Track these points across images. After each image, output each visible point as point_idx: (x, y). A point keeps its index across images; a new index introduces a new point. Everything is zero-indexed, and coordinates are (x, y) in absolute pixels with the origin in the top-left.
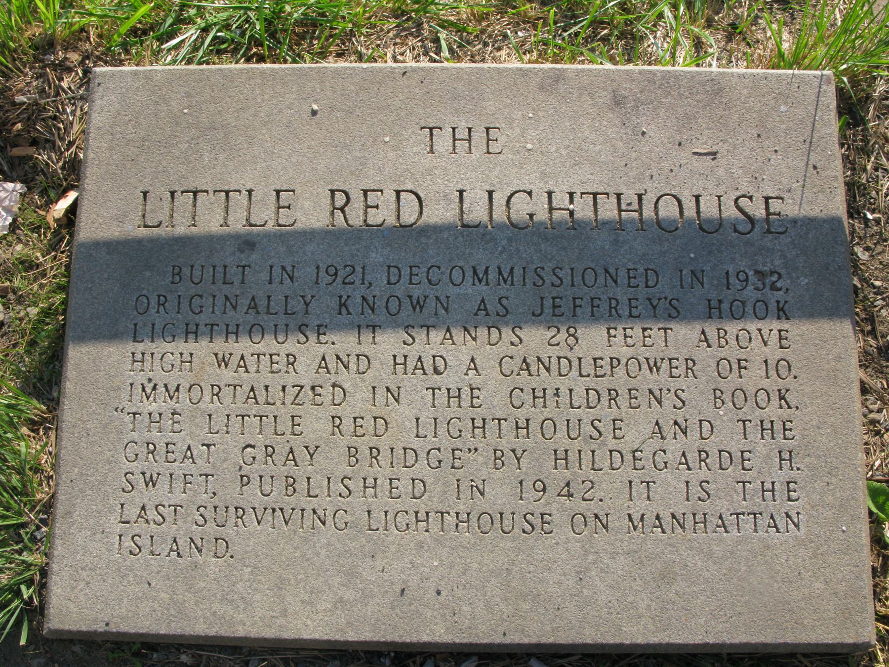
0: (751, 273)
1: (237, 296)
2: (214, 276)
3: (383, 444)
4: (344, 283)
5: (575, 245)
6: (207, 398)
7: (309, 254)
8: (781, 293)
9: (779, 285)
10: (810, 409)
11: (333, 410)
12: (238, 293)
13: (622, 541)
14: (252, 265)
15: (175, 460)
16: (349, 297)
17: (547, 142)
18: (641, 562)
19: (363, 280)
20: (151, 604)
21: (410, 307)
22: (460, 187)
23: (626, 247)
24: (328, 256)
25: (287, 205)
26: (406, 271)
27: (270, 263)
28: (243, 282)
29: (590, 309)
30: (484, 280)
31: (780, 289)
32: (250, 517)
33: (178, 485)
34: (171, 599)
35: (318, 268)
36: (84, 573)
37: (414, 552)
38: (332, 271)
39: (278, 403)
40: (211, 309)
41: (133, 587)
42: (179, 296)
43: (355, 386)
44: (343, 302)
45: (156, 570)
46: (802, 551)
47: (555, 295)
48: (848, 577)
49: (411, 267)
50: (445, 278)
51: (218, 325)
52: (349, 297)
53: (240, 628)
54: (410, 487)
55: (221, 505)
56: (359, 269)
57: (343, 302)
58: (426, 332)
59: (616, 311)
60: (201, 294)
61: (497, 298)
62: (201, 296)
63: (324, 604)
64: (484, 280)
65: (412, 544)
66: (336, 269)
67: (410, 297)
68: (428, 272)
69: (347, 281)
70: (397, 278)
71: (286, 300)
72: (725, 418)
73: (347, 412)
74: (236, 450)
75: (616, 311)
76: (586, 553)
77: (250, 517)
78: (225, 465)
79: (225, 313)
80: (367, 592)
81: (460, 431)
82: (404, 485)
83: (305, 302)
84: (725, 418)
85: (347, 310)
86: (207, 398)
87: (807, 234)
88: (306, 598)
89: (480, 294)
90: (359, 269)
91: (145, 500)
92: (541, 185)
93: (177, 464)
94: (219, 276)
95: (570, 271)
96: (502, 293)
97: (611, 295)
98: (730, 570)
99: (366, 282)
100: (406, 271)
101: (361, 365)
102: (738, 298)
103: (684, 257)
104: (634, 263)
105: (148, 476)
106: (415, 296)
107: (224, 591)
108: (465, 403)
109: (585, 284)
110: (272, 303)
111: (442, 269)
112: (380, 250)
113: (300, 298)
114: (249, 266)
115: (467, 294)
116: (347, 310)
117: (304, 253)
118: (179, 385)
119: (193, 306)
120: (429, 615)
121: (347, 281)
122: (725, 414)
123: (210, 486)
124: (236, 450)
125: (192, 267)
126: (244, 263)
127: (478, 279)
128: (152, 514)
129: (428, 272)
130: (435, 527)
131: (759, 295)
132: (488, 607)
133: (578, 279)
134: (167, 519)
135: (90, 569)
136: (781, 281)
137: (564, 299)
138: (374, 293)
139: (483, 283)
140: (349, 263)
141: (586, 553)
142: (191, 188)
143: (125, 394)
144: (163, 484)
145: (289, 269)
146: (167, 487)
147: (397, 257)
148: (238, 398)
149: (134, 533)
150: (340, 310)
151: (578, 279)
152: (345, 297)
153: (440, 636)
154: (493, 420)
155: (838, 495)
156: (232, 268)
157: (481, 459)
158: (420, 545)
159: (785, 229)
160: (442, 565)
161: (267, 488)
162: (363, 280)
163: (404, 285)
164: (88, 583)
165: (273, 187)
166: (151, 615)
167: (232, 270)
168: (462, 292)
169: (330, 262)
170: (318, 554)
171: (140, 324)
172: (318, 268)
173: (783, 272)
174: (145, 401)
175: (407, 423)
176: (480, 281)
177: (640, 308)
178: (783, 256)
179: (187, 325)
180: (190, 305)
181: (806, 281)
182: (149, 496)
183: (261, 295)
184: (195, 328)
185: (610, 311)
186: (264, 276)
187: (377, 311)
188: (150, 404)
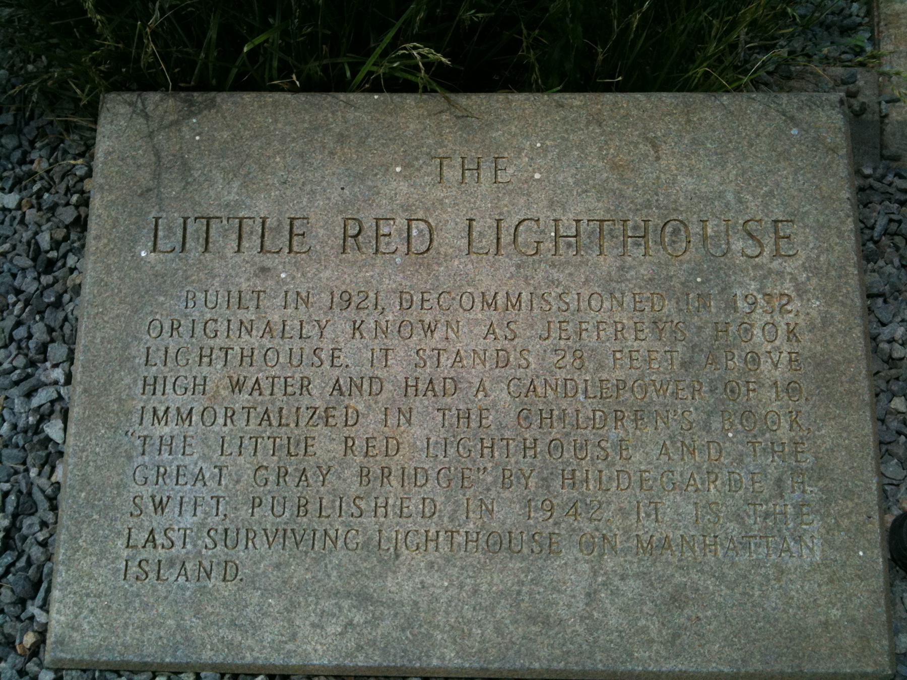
0: (759, 296)
1: (252, 321)
2: (229, 301)
3: (394, 464)
4: (357, 308)
5: (582, 271)
6: (221, 421)
7: (325, 280)
8: (791, 315)
9: (789, 308)
10: (823, 431)
11: (347, 432)
12: (253, 318)
13: (631, 562)
14: (268, 291)
15: (186, 483)
16: (362, 321)
17: (555, 170)
18: (652, 585)
19: (376, 305)
20: (155, 631)
21: (422, 332)
22: (469, 216)
23: (633, 273)
24: (344, 283)
25: (301, 232)
26: (417, 298)
27: (285, 288)
28: (258, 307)
29: (596, 333)
30: (493, 305)
31: (790, 312)
32: (260, 541)
33: (188, 508)
34: (178, 626)
35: (332, 293)
36: (89, 600)
37: (424, 572)
38: (346, 297)
39: (292, 425)
40: (226, 334)
41: (139, 613)
42: (194, 321)
43: (369, 407)
44: (357, 326)
45: (164, 595)
46: (818, 577)
47: (562, 320)
48: (865, 603)
49: (422, 293)
50: (456, 304)
51: (232, 349)
52: (362, 321)
53: (248, 655)
54: (421, 506)
55: (232, 527)
56: (372, 295)
57: (357, 326)
58: (61, 425)
59: (622, 334)
60: (215, 318)
61: (506, 323)
62: (216, 321)
63: (333, 628)
64: (493, 305)
65: (422, 564)
66: (350, 294)
67: (422, 321)
68: (439, 298)
69: (361, 306)
70: (409, 304)
71: (301, 325)
72: (735, 440)
73: (360, 433)
74: (249, 472)
75: (622, 334)
76: (595, 574)
77: (260, 541)
78: (238, 487)
79: (240, 337)
80: (377, 613)
81: (470, 451)
82: (414, 505)
83: (320, 326)
84: (735, 440)
85: (361, 334)
86: (221, 421)
87: (818, 257)
88: (316, 621)
89: (489, 319)
90: (372, 295)
91: (155, 524)
92: (549, 213)
93: (189, 486)
94: (234, 301)
95: (576, 297)
96: (510, 318)
97: (617, 320)
98: (744, 594)
99: (379, 307)
100: (417, 298)
101: (374, 387)
102: (746, 320)
103: (691, 281)
104: (640, 288)
105: (157, 499)
106: (427, 321)
107: (232, 615)
108: (473, 425)
109: (591, 309)
110: (287, 328)
111: (453, 295)
112: (393, 277)
113: (315, 323)
114: (264, 292)
115: (477, 319)
116: (361, 334)
117: (320, 279)
118: (192, 409)
119: (207, 331)
120: (439, 637)
121: (361, 306)
122: (734, 436)
123: (221, 508)
124: (249, 472)
125: (206, 291)
126: (259, 288)
127: (487, 304)
128: (159, 539)
129: (439, 298)
130: (445, 549)
131: (768, 318)
132: (498, 630)
133: (584, 305)
134: (176, 543)
135: (95, 596)
136: (791, 304)
137: (571, 324)
138: (387, 318)
139: (492, 309)
140: (363, 289)
141: (595, 574)
142: (205, 215)
143: (136, 418)
144: (172, 509)
145: (304, 294)
146: (177, 510)
147: (409, 284)
148: (252, 421)
149: (141, 557)
150: (354, 334)
151: (584, 305)
152: (359, 322)
153: (450, 660)
154: (502, 440)
155: (854, 519)
156: (247, 293)
157: (490, 479)
158: (431, 565)
159: (795, 251)
160: (451, 584)
161: (278, 509)
162: (376, 305)
163: (416, 310)
164: (92, 611)
165: (287, 215)
166: (157, 643)
167: (246, 296)
168: (471, 317)
169: (344, 288)
170: (329, 576)
171: (153, 348)
172: (332, 293)
173: (793, 295)
174: (157, 425)
175: (418, 443)
176: (489, 306)
177: (646, 331)
178: (794, 279)
179: (201, 349)
180: (205, 330)
181: (818, 303)
182: (158, 522)
183: (276, 318)
184: (209, 351)
185: (616, 335)
186: (279, 301)
187: (390, 336)
188: (162, 428)
